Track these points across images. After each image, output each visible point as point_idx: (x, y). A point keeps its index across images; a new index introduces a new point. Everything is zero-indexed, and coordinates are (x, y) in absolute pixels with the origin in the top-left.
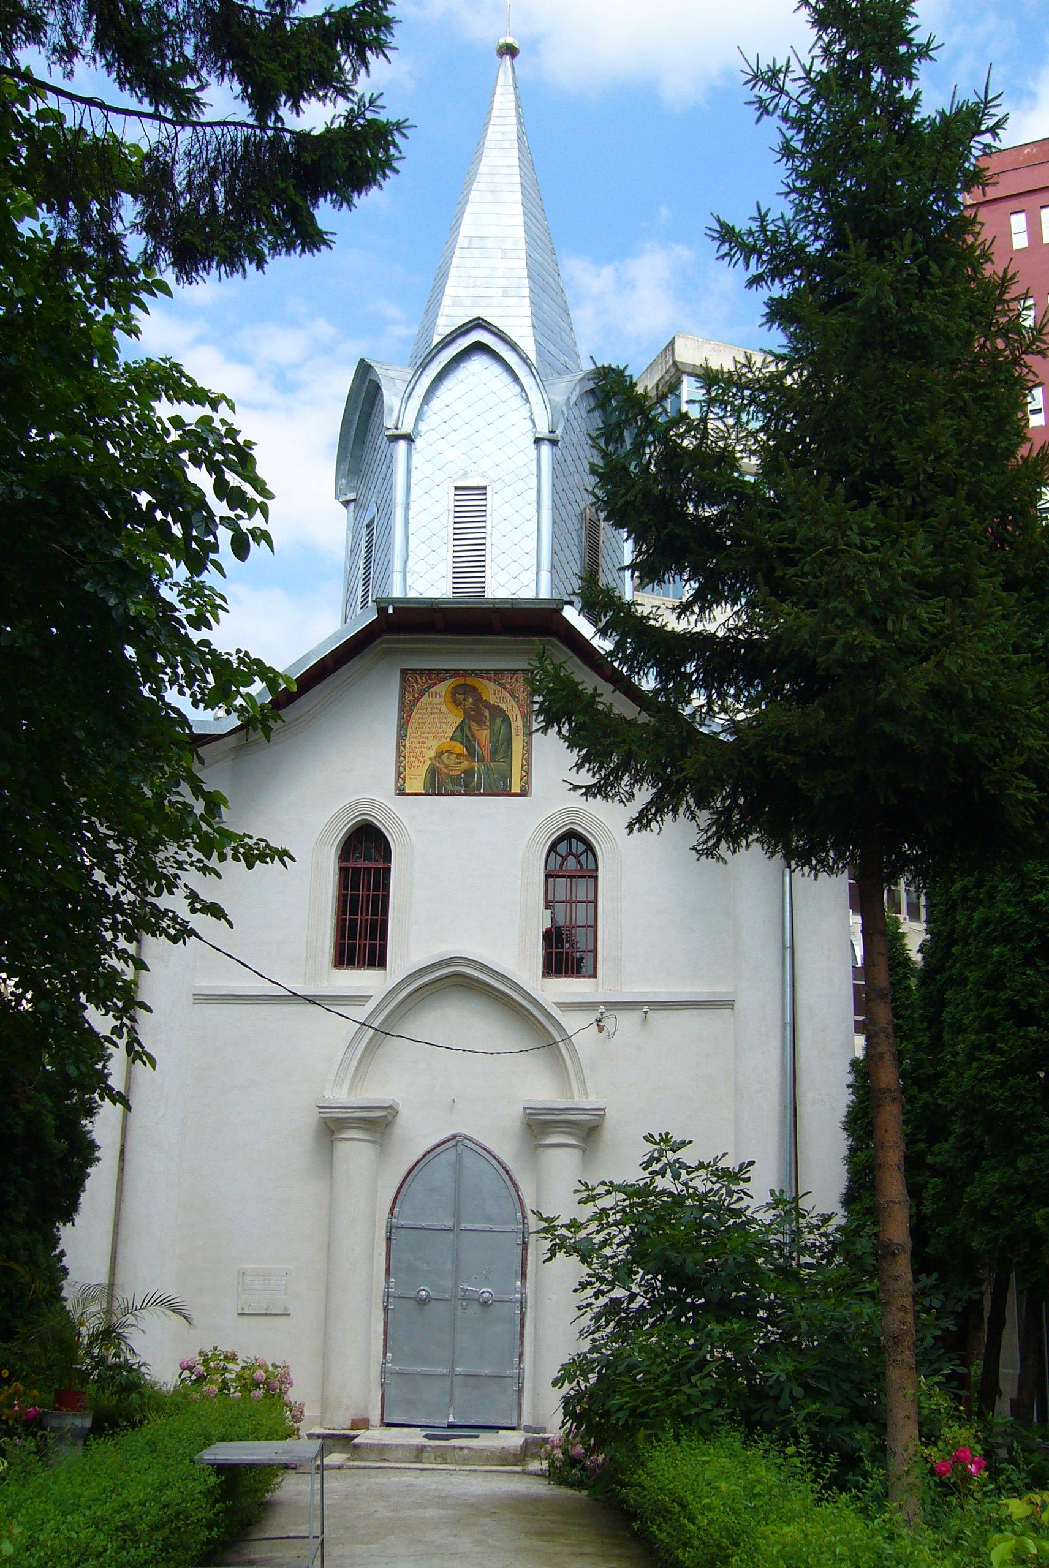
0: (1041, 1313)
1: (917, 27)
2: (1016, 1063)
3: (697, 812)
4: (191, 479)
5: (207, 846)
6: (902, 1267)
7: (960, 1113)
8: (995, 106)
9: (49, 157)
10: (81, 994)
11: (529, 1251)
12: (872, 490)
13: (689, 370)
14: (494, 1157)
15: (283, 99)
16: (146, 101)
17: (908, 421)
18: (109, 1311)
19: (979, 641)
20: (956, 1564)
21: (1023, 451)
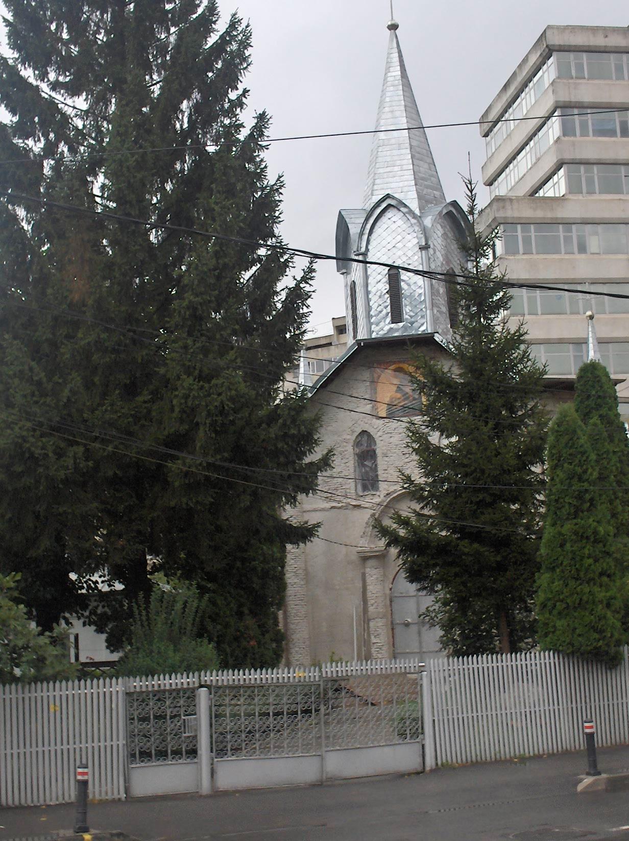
0: (357, 639)
1: (262, 119)
2: (483, 535)
3: (303, 330)
4: (294, 522)
5: (462, 355)
6: (90, 608)
7: (620, 454)
8: (17, 690)
9: (447, 451)
10: (115, 205)
11: (357, 295)
12: (225, 460)
13: (556, 48)
14: (434, 727)
15: (18, 577)
16: (11, 14)
17: (571, 447)
18: (306, 562)
19: (125, 81)
20: (625, 530)
21: (18, 577)
